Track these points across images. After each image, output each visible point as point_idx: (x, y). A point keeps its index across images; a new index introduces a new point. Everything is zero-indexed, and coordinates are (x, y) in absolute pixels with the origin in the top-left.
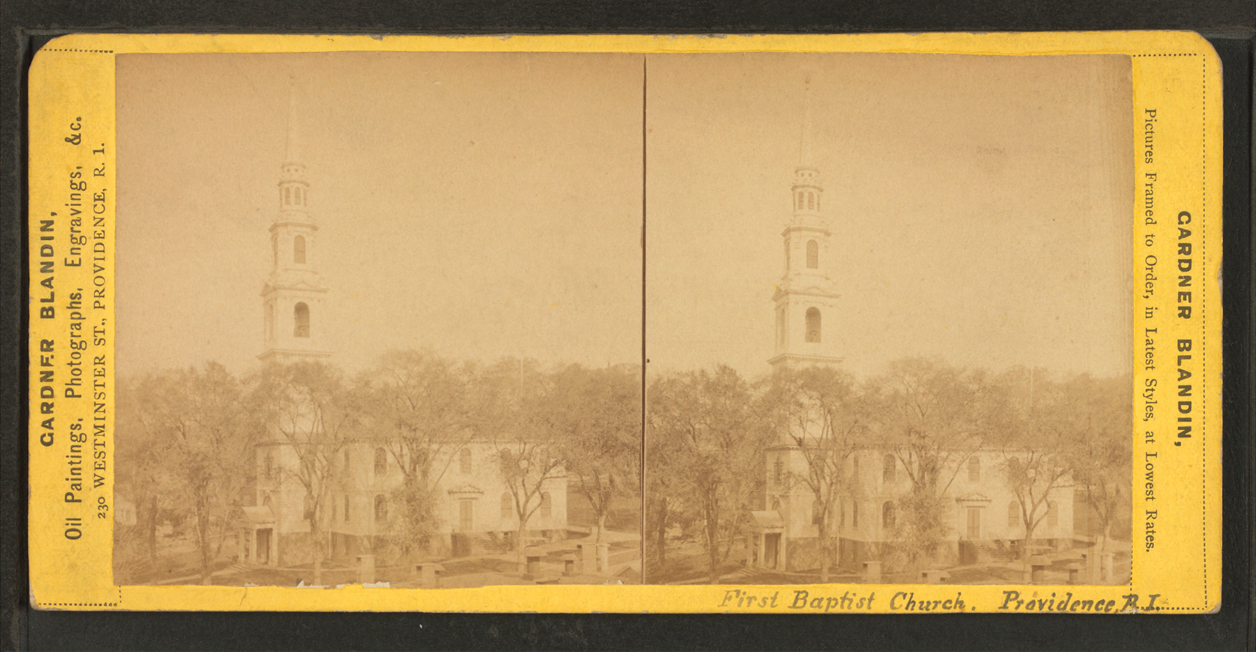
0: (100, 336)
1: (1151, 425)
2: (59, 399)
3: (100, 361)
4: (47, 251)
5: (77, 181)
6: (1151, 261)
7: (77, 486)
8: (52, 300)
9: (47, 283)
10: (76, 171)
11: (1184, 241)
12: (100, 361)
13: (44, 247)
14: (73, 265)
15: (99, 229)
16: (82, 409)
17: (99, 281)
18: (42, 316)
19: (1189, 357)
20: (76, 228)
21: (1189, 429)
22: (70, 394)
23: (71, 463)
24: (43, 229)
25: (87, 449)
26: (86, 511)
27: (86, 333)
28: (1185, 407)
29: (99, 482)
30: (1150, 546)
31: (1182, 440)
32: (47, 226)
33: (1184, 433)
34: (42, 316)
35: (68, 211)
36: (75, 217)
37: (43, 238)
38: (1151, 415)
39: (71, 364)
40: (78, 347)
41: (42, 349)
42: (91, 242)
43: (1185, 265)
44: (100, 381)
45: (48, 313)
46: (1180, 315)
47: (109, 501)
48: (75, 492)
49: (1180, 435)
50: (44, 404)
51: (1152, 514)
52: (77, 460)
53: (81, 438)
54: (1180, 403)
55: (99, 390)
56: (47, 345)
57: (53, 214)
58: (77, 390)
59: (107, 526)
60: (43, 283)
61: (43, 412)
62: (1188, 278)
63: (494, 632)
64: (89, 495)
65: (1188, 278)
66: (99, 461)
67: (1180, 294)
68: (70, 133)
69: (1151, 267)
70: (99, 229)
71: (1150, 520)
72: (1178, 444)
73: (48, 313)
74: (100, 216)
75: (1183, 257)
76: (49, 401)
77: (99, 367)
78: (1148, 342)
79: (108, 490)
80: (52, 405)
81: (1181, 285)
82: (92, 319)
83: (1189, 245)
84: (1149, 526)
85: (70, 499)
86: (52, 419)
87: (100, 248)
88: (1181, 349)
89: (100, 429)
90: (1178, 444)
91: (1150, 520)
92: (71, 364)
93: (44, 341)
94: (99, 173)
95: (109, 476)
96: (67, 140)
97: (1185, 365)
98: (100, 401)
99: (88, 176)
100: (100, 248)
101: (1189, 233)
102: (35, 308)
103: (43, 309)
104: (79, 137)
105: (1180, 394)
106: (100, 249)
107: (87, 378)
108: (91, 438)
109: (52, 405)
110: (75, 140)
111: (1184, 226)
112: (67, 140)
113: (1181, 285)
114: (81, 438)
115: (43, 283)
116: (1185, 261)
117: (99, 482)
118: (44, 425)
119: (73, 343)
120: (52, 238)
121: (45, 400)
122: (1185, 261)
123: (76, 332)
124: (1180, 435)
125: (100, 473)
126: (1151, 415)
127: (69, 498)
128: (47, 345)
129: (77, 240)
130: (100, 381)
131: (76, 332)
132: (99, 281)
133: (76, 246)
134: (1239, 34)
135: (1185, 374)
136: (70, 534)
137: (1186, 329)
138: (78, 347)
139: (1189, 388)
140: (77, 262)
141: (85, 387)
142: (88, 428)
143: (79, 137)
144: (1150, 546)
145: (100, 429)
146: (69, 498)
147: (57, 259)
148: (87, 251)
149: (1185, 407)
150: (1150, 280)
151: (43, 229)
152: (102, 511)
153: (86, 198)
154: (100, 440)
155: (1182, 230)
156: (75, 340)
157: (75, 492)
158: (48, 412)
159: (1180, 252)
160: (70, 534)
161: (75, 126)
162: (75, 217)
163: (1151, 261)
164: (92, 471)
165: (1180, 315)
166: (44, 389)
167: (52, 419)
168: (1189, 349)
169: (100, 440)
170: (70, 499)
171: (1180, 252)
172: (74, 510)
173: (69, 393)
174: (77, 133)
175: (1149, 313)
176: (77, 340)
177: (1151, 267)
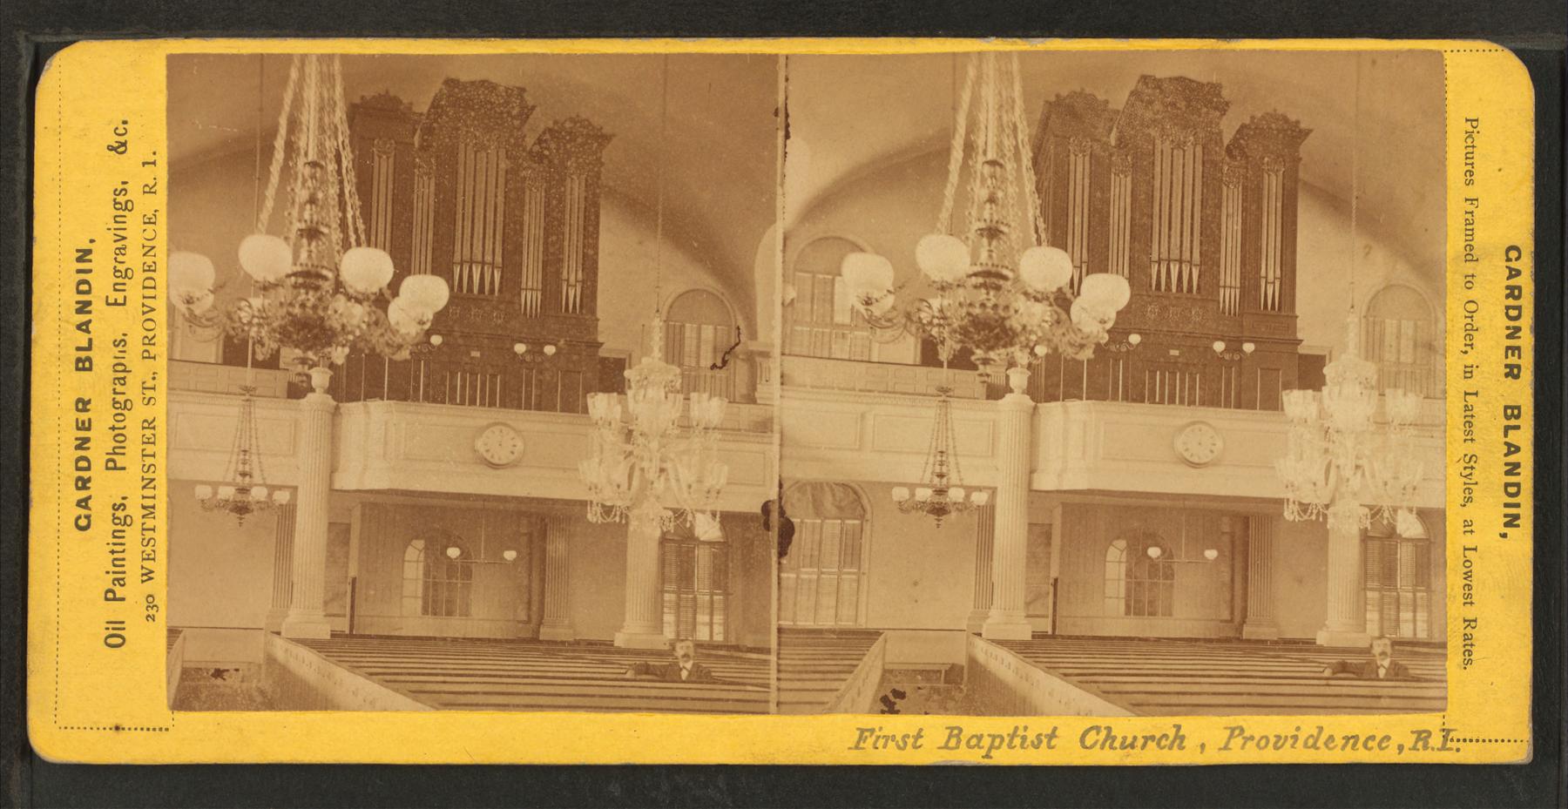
0: (149, 393)
1: (1471, 512)
2: (97, 473)
3: (149, 424)
4: (84, 287)
5: (121, 199)
6: (1472, 307)
7: (120, 581)
8: (89, 348)
9: (1512, 449)
10: (120, 187)
11: (1512, 282)
12: (149, 424)
13: (1517, 494)
14: (116, 303)
15: (149, 260)
16: (127, 484)
18: (1519, 408)
20: (120, 258)
21: (79, 260)
22: (112, 466)
23: (113, 552)
24: (1517, 517)
25: (132, 536)
26: (130, 611)
27: (132, 391)
28: (1512, 490)
29: (148, 576)
31: (87, 246)
32: (1512, 521)
34: (1519, 408)
35: (110, 236)
36: (119, 244)
37: (79, 271)
38: (1470, 499)
39: (113, 428)
40: (121, 407)
41: (1519, 367)
42: (139, 276)
43: (1513, 313)
44: (150, 449)
45: (1512, 412)
46: (1507, 375)
47: (161, 600)
48: (117, 589)
49: (1506, 525)
50: (1519, 297)
51: (1470, 622)
54: (1507, 485)
56: (1512, 372)
57: (1504, 536)
58: (120, 460)
59: (160, 629)
60: (1518, 449)
61: (78, 488)
62: (78, 447)
64: (134, 589)
65: (78, 447)
66: (148, 549)
68: (113, 140)
69: (1471, 315)
70: (149, 260)
71: (1469, 630)
72: (92, 241)
73: (1512, 412)
75: (1511, 302)
76: (85, 475)
77: (148, 433)
79: (159, 587)
80: (89, 480)
81: (1508, 337)
83: (1519, 288)
85: (111, 596)
86: (89, 498)
87: (150, 283)
88: (1507, 417)
89: (149, 510)
90: (1504, 536)
91: (1469, 630)
92: (113, 428)
93: (1517, 377)
94: (150, 190)
95: (160, 567)
96: (111, 148)
97: (1513, 437)
98: (150, 475)
99: (134, 193)
100: (150, 283)
101: (79, 504)
104: (124, 144)
106: (149, 286)
107: (133, 447)
108: (138, 521)
109: (89, 480)
110: (119, 148)
111: (1513, 265)
112: (111, 148)
113: (1508, 337)
114: (126, 522)
115: (1518, 449)
116: (1514, 308)
117: (148, 576)
118: (79, 504)
119: (115, 402)
120: (1506, 505)
121: (81, 474)
122: (1514, 308)
124: (1506, 525)
125: (147, 564)
126: (1470, 499)
127: (110, 595)
128: (1512, 372)
130: (150, 449)
132: (149, 325)
133: (120, 280)
134: (1550, 43)
135: (83, 327)
136: (110, 641)
137: (84, 384)
138: (121, 407)
139: (79, 311)
140: (121, 301)
141: (131, 458)
142: (134, 510)
143: (124, 144)
145: (149, 510)
146: (110, 595)
147: (97, 299)
148: (134, 291)
149: (1512, 490)
150: (1470, 331)
151: (1517, 517)
152: (151, 612)
153: (133, 222)
154: (150, 523)
155: (86, 507)
156: (118, 398)
157: (117, 589)
158: (84, 487)
159: (1507, 297)
160: (110, 641)
161: (121, 131)
162: (119, 244)
163: (1472, 307)
164: (140, 563)
165: (1507, 375)
166: (1518, 318)
167: (89, 498)
168: (79, 360)
169: (150, 523)
170: (111, 596)
171: (1507, 297)
172: (115, 611)
173: (111, 465)
174: (122, 139)
175: (1468, 373)
176: (120, 398)
177: (1471, 315)
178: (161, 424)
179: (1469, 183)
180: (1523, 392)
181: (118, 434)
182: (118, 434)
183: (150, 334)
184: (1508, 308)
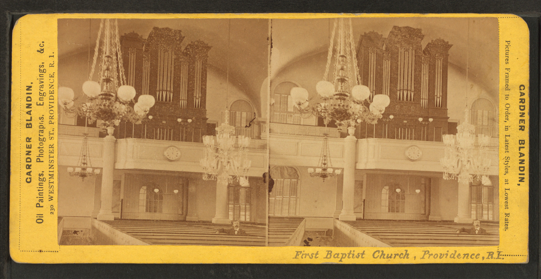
0: (51, 136)
1: (507, 176)
2: (34, 163)
3: (51, 146)
5: (42, 69)
6: (508, 106)
7: (41, 200)
9: (522, 155)
10: (41, 64)
12: (51, 146)
14: (40, 105)
16: (44, 167)
17: (52, 112)
18: (524, 141)
19: (27, 120)
20: (41, 89)
21: (27, 90)
22: (39, 161)
24: (523, 178)
25: (46, 185)
26: (45, 211)
27: (46, 135)
28: (522, 169)
29: (51, 199)
30: (506, 228)
31: (30, 85)
32: (522, 180)
33: (29, 88)
34: (524, 141)
35: (38, 81)
36: (41, 84)
37: (27, 94)
38: (507, 172)
39: (39, 148)
40: (42, 140)
41: (524, 127)
42: (48, 95)
43: (522, 108)
44: (52, 155)
45: (522, 142)
46: (520, 129)
47: (56, 207)
48: (40, 203)
49: (520, 181)
50: (524, 103)
51: (507, 215)
52: (41, 189)
53: (43, 180)
54: (520, 167)
55: (51, 159)
56: (522, 128)
58: (41, 159)
60: (524, 155)
61: (27, 168)
62: (27, 154)
63: (212, 272)
64: (46, 203)
65: (27, 154)
66: (51, 190)
67: (520, 120)
68: (39, 48)
71: (507, 217)
73: (522, 142)
74: (52, 84)
75: (521, 104)
76: (29, 164)
77: (51, 149)
78: (506, 141)
79: (55, 202)
80: (31, 165)
82: (48, 128)
83: (524, 99)
84: (506, 220)
85: (38, 206)
86: (31, 172)
87: (52, 98)
88: (520, 144)
89: (51, 176)
90: (519, 185)
91: (507, 217)
92: (39, 148)
93: (523, 130)
94: (52, 66)
95: (55, 196)
96: (38, 51)
97: (522, 151)
98: (52, 164)
99: (46, 66)
100: (52, 98)
101: (27, 174)
102: (527, 145)
103: (27, 124)
104: (43, 50)
105: (520, 163)
106: (51, 99)
107: (46, 154)
108: (48, 180)
109: (31, 165)
110: (41, 51)
111: (29, 177)
112: (38, 51)
114: (43, 180)
115: (524, 155)
117: (51, 199)
118: (27, 174)
120: (520, 174)
122: (522, 106)
123: (41, 134)
124: (520, 181)
125: (51, 195)
126: (507, 172)
127: (38, 205)
128: (522, 128)
129: (42, 95)
130: (52, 155)
131: (41, 134)
132: (52, 112)
133: (41, 97)
134: (535, 15)
135: (29, 113)
136: (38, 221)
137: (29, 133)
138: (42, 140)
139: (27, 107)
140: (42, 104)
141: (45, 158)
142: (46, 176)
143: (43, 50)
144: (506, 228)
145: (51, 176)
146: (38, 205)
147: (33, 103)
148: (46, 100)
149: (522, 169)
150: (507, 114)
151: (523, 178)
152: (52, 211)
154: (52, 180)
155: (30, 175)
156: (41, 137)
157: (40, 203)
158: (29, 168)
159: (520, 102)
160: (38, 221)
161: (42, 45)
162: (41, 84)
163: (508, 106)
164: (48, 194)
165: (520, 129)
166: (524, 110)
167: (31, 172)
168: (27, 124)
169: (52, 180)
170: (38, 206)
171: (520, 102)
172: (40, 211)
173: (38, 160)
174: (42, 48)
175: (507, 128)
176: (41, 137)
178: (56, 146)
179: (507, 63)
180: (525, 135)
181: (41, 149)
182: (41, 149)
183: (52, 115)
184: (520, 106)
